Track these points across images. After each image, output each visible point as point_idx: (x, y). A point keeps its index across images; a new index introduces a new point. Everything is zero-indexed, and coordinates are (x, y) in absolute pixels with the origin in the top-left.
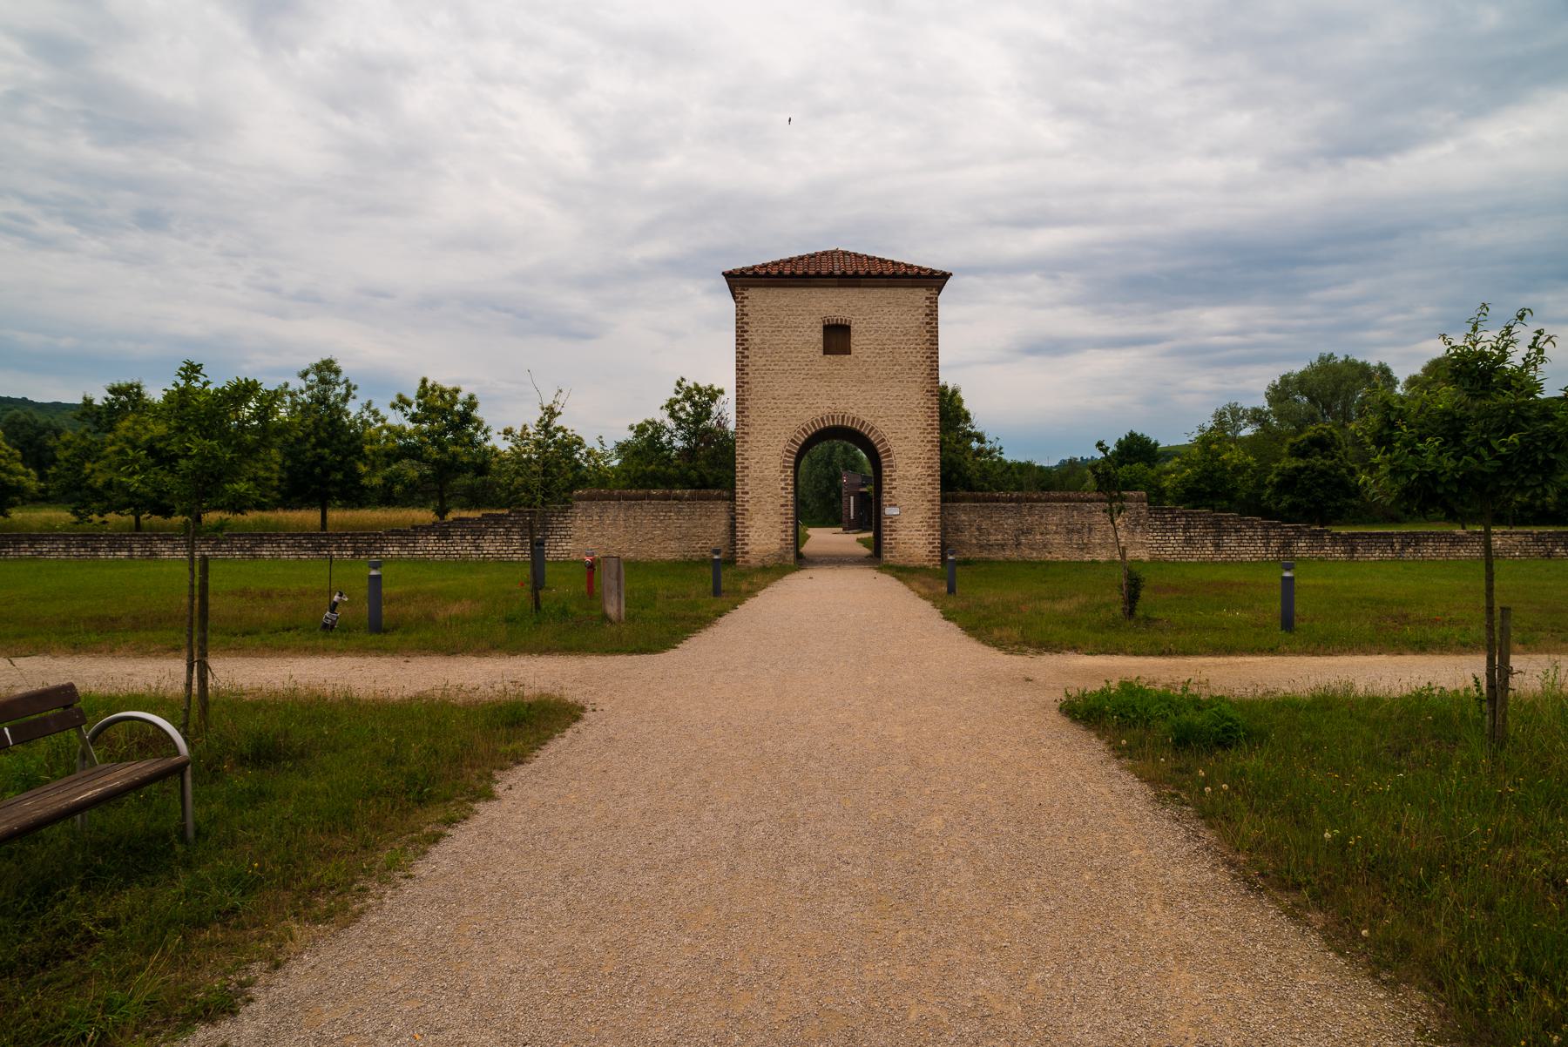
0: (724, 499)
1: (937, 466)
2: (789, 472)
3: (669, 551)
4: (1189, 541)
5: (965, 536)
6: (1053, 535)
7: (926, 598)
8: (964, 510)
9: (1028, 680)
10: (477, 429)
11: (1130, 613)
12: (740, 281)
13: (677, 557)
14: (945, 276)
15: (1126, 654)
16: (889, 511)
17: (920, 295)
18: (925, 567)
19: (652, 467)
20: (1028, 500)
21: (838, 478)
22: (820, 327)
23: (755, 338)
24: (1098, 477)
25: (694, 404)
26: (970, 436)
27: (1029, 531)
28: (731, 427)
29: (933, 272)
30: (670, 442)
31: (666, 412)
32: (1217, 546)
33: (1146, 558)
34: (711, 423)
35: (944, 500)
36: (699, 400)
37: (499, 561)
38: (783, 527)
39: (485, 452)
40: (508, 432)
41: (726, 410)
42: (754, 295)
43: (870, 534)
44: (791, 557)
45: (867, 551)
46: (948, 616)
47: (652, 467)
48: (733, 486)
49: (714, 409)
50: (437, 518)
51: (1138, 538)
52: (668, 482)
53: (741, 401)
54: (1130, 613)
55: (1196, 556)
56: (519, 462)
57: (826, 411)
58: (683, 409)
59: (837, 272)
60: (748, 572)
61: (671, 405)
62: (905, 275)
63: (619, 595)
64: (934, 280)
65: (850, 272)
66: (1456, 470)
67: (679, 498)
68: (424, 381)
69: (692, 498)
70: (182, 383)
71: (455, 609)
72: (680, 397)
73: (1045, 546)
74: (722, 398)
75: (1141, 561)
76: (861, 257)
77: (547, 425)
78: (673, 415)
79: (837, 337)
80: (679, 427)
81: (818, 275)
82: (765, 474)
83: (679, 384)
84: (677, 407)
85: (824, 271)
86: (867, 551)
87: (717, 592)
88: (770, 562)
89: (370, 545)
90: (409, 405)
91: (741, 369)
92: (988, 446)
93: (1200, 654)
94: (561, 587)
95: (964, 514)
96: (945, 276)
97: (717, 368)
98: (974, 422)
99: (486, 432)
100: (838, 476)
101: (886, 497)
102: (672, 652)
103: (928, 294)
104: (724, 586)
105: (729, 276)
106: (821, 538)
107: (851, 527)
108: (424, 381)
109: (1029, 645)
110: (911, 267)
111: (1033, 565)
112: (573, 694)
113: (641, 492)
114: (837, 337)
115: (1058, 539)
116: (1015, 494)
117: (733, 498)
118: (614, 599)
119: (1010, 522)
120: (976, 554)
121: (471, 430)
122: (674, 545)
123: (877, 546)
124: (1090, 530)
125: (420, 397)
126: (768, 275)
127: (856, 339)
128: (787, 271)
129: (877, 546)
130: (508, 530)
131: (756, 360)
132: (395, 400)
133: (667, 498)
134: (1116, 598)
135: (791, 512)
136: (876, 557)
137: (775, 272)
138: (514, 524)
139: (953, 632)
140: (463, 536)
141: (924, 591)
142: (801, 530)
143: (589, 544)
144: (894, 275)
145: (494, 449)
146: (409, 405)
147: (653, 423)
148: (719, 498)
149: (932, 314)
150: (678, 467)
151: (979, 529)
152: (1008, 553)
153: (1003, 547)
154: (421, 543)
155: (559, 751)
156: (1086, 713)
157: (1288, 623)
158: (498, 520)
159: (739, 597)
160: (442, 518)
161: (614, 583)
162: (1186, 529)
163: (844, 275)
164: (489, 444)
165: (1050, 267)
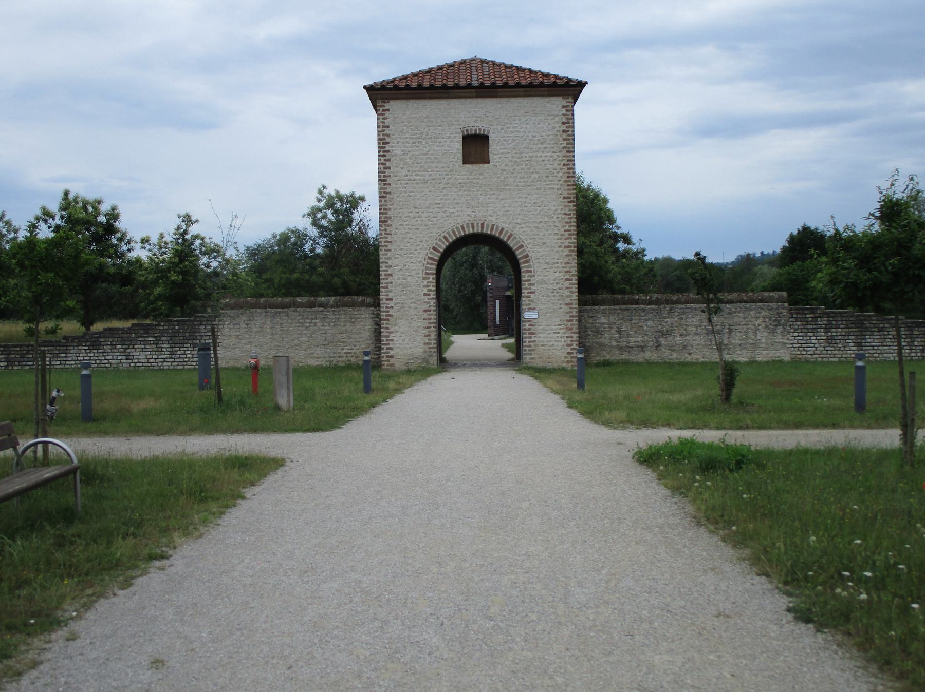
0: (368, 305)
1: (574, 271)
2: (432, 278)
3: (318, 356)
4: (830, 341)
5: (606, 339)
6: (690, 335)
7: (556, 393)
8: (604, 312)
9: (620, 443)
10: (121, 240)
11: (727, 398)
12: (380, 94)
13: (324, 362)
14: (581, 85)
15: (710, 429)
16: (527, 315)
17: (556, 104)
18: (563, 369)
19: (296, 275)
20: (668, 302)
21: (478, 284)
22: (460, 138)
23: (396, 149)
24: (696, 282)
25: (336, 212)
26: (616, 237)
27: (669, 333)
28: (373, 232)
29: (569, 80)
30: (313, 250)
31: (309, 220)
32: (859, 345)
33: (787, 358)
34: (353, 230)
35: (582, 303)
36: (344, 207)
37: (150, 370)
38: (426, 331)
39: (130, 262)
40: (145, 241)
41: (369, 216)
42: (396, 107)
43: (512, 341)
44: (434, 360)
45: (511, 355)
46: (571, 406)
47: (296, 275)
48: (377, 293)
49: (356, 216)
50: (83, 329)
51: (779, 338)
52: (312, 289)
53: (383, 211)
54: (727, 398)
55: (838, 355)
56: (159, 271)
57: (466, 219)
58: (324, 217)
59: (475, 83)
60: (394, 375)
61: (313, 213)
62: (542, 85)
63: (288, 388)
64: (571, 89)
65: (487, 83)
66: (867, 281)
67: (322, 305)
68: (66, 194)
69: (337, 305)
70: (29, 235)
71: (144, 404)
72: (322, 204)
73: (685, 347)
74: (363, 206)
75: (781, 362)
76: (499, 65)
77: (185, 233)
78: (315, 223)
79: (476, 146)
80: (321, 235)
81: (457, 87)
82: (408, 281)
83: (320, 192)
84: (319, 215)
85: (463, 83)
86: (511, 355)
87: (367, 389)
88: (413, 366)
89: (22, 356)
90: (53, 217)
91: (383, 180)
92: (634, 248)
93: (770, 428)
94: (232, 388)
95: (605, 318)
96: (581, 85)
97: (354, 170)
98: (618, 223)
99: (129, 242)
100: (483, 279)
101: (525, 301)
102: (338, 430)
103: (564, 103)
104: (374, 385)
105: (370, 89)
106: (465, 344)
107: (496, 332)
108: (66, 194)
109: (632, 423)
110: (548, 75)
111: (670, 365)
112: (274, 453)
113: (287, 300)
114: (476, 146)
115: (698, 340)
116: (655, 296)
117: (377, 305)
118: (284, 392)
119: (649, 324)
120: (615, 356)
121: (114, 241)
122: (320, 351)
123: (518, 349)
124: (730, 331)
125: (63, 208)
126: (408, 87)
127: (494, 147)
128: (426, 84)
129: (518, 349)
130: (158, 340)
131: (397, 171)
132: (39, 213)
133: (311, 305)
134: (716, 390)
135: (433, 316)
136: (516, 359)
137: (414, 85)
138: (163, 333)
139: (573, 416)
140: (113, 346)
141: (557, 387)
142: (444, 336)
143: (237, 351)
144: (531, 85)
145: (138, 260)
146: (53, 217)
147: (295, 232)
148: (363, 304)
149: (568, 123)
150: (322, 274)
151: (619, 331)
152: (648, 355)
153: (642, 348)
154: (72, 354)
155: (273, 479)
156: (649, 458)
157: (860, 406)
158: (147, 329)
159: (387, 395)
160: (88, 329)
161: (284, 379)
162: (828, 329)
163: (482, 86)
164: (132, 255)
165: (727, 36)
